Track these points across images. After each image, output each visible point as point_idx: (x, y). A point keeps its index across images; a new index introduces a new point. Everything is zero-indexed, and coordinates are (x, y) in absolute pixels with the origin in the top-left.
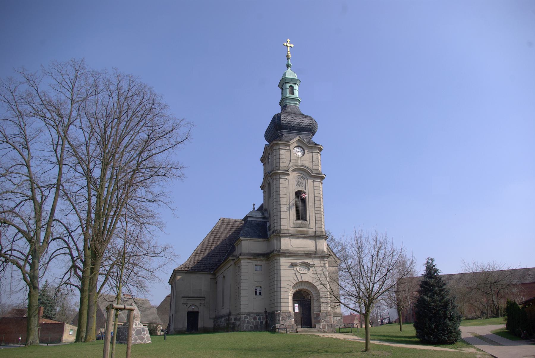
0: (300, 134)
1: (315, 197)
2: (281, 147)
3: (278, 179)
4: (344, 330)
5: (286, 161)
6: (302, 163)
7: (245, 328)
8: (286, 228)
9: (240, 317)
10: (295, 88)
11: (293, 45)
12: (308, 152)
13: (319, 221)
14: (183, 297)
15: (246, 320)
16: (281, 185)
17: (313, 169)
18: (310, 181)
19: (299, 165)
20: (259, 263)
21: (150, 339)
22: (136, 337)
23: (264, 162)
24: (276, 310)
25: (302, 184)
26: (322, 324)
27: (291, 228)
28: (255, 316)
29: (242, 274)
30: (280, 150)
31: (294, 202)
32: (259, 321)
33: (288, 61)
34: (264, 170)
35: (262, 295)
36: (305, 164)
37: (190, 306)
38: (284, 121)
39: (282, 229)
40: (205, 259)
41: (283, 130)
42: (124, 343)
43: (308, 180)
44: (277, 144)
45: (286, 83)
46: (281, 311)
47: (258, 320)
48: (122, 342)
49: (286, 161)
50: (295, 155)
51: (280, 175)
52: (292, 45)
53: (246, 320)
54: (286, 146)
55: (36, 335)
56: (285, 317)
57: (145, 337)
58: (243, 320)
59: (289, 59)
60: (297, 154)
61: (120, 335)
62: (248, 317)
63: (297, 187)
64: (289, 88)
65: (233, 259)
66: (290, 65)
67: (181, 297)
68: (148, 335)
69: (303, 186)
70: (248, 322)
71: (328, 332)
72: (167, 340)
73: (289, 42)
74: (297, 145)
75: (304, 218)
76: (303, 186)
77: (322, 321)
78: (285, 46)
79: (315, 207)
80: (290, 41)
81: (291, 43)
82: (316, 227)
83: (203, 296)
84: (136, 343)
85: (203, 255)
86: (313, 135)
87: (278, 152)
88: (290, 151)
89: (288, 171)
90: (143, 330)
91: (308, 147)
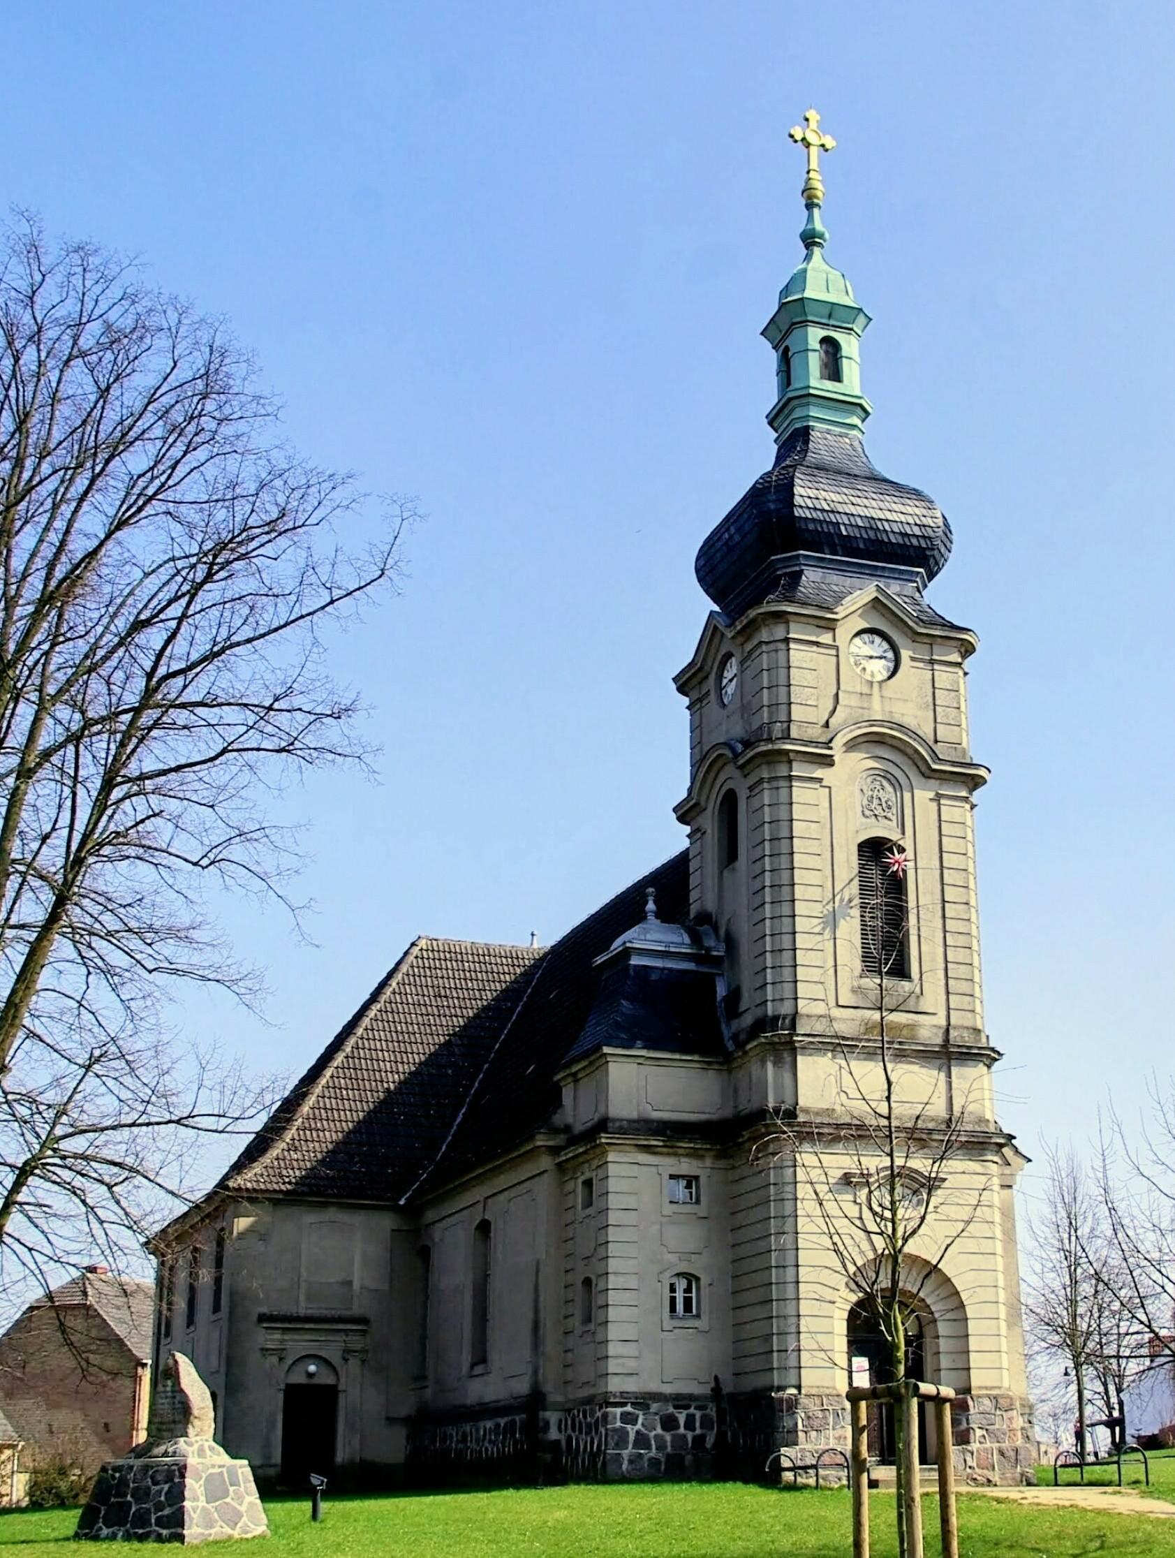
0: (874, 573)
1: (945, 871)
2: (796, 633)
3: (783, 783)
4: (1073, 1474)
5: (818, 700)
6: (887, 708)
7: (624, 1467)
8: (820, 1008)
9: (599, 1414)
10: (845, 351)
11: (834, 138)
12: (913, 659)
13: (963, 982)
14: (262, 1318)
15: (632, 1430)
16: (797, 812)
17: (936, 741)
18: (923, 794)
19: (872, 722)
20: (686, 1166)
21: (263, 1516)
22: (209, 1506)
23: (695, 695)
24: (776, 1384)
25: (889, 807)
26: (974, 1446)
27: (836, 1012)
28: (671, 1410)
29: (613, 1218)
30: (792, 645)
31: (855, 888)
32: (690, 1436)
33: (810, 218)
34: (696, 728)
35: (698, 1316)
36: (903, 715)
37: (298, 1360)
38: (807, 512)
39: (802, 1015)
40: (361, 1134)
41: (802, 552)
42: (153, 1536)
43: (916, 791)
44: (780, 617)
45: (805, 323)
46: (799, 1388)
47: (682, 1430)
48: (140, 1531)
49: (818, 700)
50: (858, 670)
51: (790, 762)
52: (830, 142)
53: (629, 1427)
54: (818, 626)
55: (660, 1502)
56: (820, 1415)
57: (243, 1509)
58: (615, 1430)
59: (817, 205)
60: (866, 666)
61: (129, 1498)
62: (638, 1416)
63: (864, 820)
64: (818, 346)
65: (551, 1143)
66: (821, 236)
67: (255, 1318)
68: (253, 1496)
69: (890, 820)
70: (642, 1441)
71: (1005, 1483)
72: (322, 1522)
73: (813, 124)
74: (866, 625)
75: (901, 970)
76: (894, 818)
77: (979, 1433)
78: (796, 141)
79: (944, 917)
80: (818, 118)
81: (823, 129)
82: (948, 1009)
83: (357, 1310)
84: (210, 1535)
85: (349, 1118)
86: (931, 576)
87: (780, 653)
88: (834, 652)
89: (828, 744)
90: (232, 1472)
91: (915, 636)
